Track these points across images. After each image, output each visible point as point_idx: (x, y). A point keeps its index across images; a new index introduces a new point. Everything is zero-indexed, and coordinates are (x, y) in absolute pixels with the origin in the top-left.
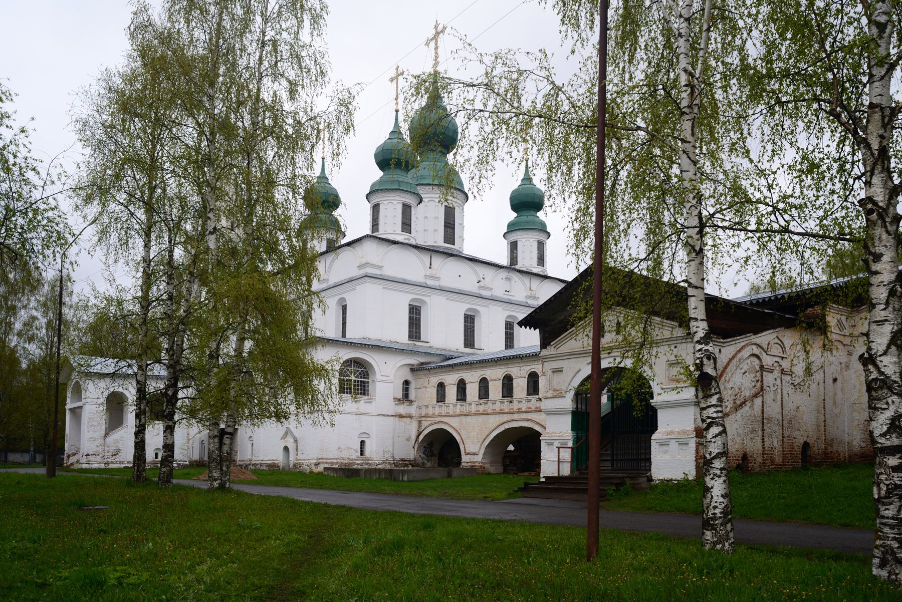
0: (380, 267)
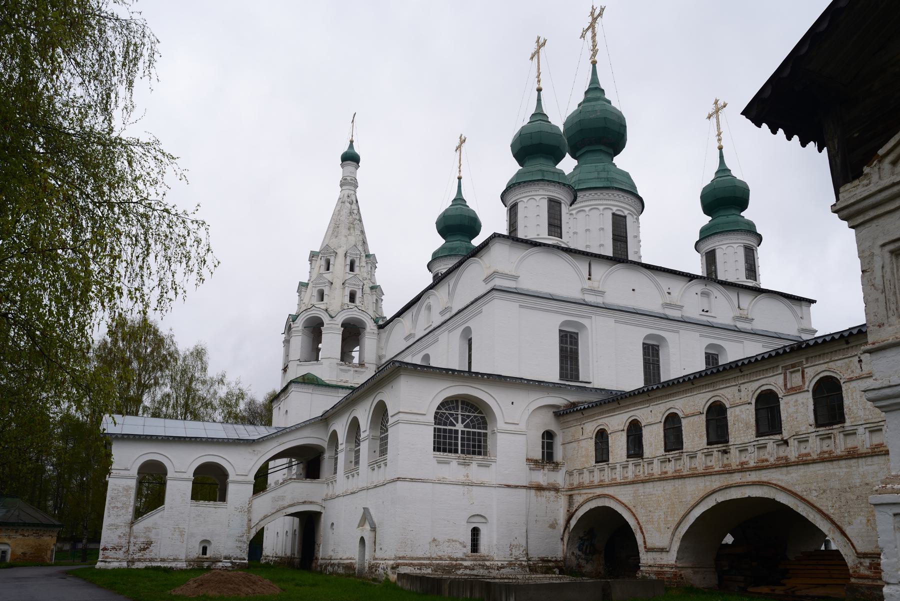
0: (515, 278)
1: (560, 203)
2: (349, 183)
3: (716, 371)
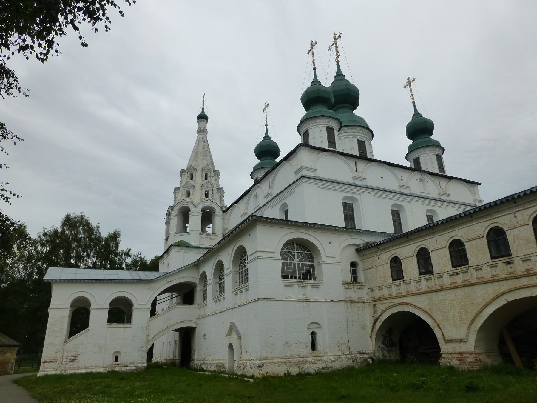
0: (314, 170)
1: (333, 129)
2: (202, 131)
3: (433, 227)
